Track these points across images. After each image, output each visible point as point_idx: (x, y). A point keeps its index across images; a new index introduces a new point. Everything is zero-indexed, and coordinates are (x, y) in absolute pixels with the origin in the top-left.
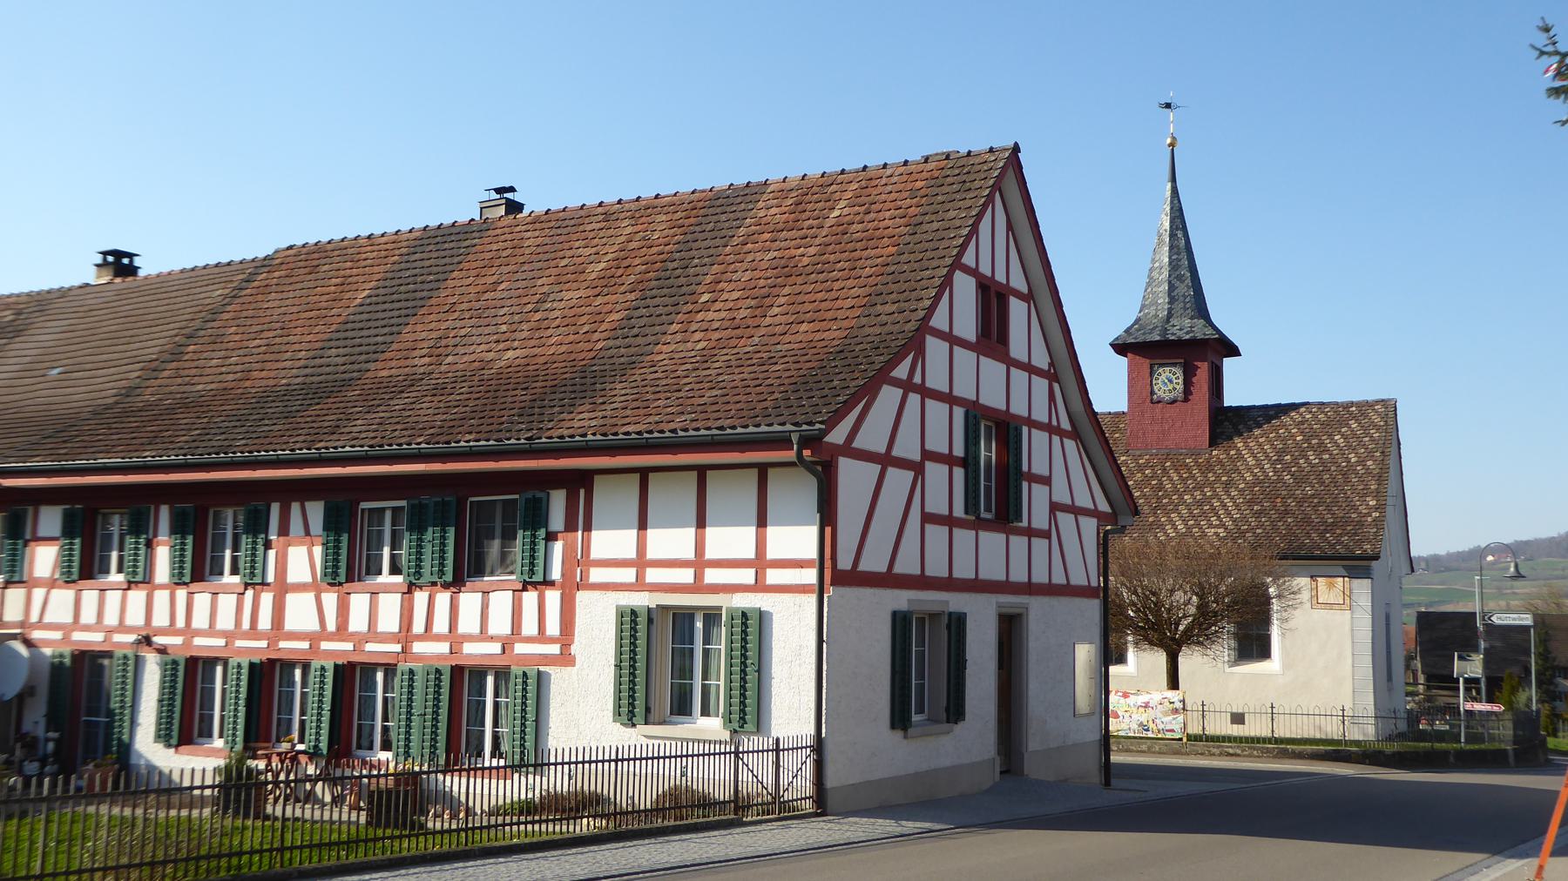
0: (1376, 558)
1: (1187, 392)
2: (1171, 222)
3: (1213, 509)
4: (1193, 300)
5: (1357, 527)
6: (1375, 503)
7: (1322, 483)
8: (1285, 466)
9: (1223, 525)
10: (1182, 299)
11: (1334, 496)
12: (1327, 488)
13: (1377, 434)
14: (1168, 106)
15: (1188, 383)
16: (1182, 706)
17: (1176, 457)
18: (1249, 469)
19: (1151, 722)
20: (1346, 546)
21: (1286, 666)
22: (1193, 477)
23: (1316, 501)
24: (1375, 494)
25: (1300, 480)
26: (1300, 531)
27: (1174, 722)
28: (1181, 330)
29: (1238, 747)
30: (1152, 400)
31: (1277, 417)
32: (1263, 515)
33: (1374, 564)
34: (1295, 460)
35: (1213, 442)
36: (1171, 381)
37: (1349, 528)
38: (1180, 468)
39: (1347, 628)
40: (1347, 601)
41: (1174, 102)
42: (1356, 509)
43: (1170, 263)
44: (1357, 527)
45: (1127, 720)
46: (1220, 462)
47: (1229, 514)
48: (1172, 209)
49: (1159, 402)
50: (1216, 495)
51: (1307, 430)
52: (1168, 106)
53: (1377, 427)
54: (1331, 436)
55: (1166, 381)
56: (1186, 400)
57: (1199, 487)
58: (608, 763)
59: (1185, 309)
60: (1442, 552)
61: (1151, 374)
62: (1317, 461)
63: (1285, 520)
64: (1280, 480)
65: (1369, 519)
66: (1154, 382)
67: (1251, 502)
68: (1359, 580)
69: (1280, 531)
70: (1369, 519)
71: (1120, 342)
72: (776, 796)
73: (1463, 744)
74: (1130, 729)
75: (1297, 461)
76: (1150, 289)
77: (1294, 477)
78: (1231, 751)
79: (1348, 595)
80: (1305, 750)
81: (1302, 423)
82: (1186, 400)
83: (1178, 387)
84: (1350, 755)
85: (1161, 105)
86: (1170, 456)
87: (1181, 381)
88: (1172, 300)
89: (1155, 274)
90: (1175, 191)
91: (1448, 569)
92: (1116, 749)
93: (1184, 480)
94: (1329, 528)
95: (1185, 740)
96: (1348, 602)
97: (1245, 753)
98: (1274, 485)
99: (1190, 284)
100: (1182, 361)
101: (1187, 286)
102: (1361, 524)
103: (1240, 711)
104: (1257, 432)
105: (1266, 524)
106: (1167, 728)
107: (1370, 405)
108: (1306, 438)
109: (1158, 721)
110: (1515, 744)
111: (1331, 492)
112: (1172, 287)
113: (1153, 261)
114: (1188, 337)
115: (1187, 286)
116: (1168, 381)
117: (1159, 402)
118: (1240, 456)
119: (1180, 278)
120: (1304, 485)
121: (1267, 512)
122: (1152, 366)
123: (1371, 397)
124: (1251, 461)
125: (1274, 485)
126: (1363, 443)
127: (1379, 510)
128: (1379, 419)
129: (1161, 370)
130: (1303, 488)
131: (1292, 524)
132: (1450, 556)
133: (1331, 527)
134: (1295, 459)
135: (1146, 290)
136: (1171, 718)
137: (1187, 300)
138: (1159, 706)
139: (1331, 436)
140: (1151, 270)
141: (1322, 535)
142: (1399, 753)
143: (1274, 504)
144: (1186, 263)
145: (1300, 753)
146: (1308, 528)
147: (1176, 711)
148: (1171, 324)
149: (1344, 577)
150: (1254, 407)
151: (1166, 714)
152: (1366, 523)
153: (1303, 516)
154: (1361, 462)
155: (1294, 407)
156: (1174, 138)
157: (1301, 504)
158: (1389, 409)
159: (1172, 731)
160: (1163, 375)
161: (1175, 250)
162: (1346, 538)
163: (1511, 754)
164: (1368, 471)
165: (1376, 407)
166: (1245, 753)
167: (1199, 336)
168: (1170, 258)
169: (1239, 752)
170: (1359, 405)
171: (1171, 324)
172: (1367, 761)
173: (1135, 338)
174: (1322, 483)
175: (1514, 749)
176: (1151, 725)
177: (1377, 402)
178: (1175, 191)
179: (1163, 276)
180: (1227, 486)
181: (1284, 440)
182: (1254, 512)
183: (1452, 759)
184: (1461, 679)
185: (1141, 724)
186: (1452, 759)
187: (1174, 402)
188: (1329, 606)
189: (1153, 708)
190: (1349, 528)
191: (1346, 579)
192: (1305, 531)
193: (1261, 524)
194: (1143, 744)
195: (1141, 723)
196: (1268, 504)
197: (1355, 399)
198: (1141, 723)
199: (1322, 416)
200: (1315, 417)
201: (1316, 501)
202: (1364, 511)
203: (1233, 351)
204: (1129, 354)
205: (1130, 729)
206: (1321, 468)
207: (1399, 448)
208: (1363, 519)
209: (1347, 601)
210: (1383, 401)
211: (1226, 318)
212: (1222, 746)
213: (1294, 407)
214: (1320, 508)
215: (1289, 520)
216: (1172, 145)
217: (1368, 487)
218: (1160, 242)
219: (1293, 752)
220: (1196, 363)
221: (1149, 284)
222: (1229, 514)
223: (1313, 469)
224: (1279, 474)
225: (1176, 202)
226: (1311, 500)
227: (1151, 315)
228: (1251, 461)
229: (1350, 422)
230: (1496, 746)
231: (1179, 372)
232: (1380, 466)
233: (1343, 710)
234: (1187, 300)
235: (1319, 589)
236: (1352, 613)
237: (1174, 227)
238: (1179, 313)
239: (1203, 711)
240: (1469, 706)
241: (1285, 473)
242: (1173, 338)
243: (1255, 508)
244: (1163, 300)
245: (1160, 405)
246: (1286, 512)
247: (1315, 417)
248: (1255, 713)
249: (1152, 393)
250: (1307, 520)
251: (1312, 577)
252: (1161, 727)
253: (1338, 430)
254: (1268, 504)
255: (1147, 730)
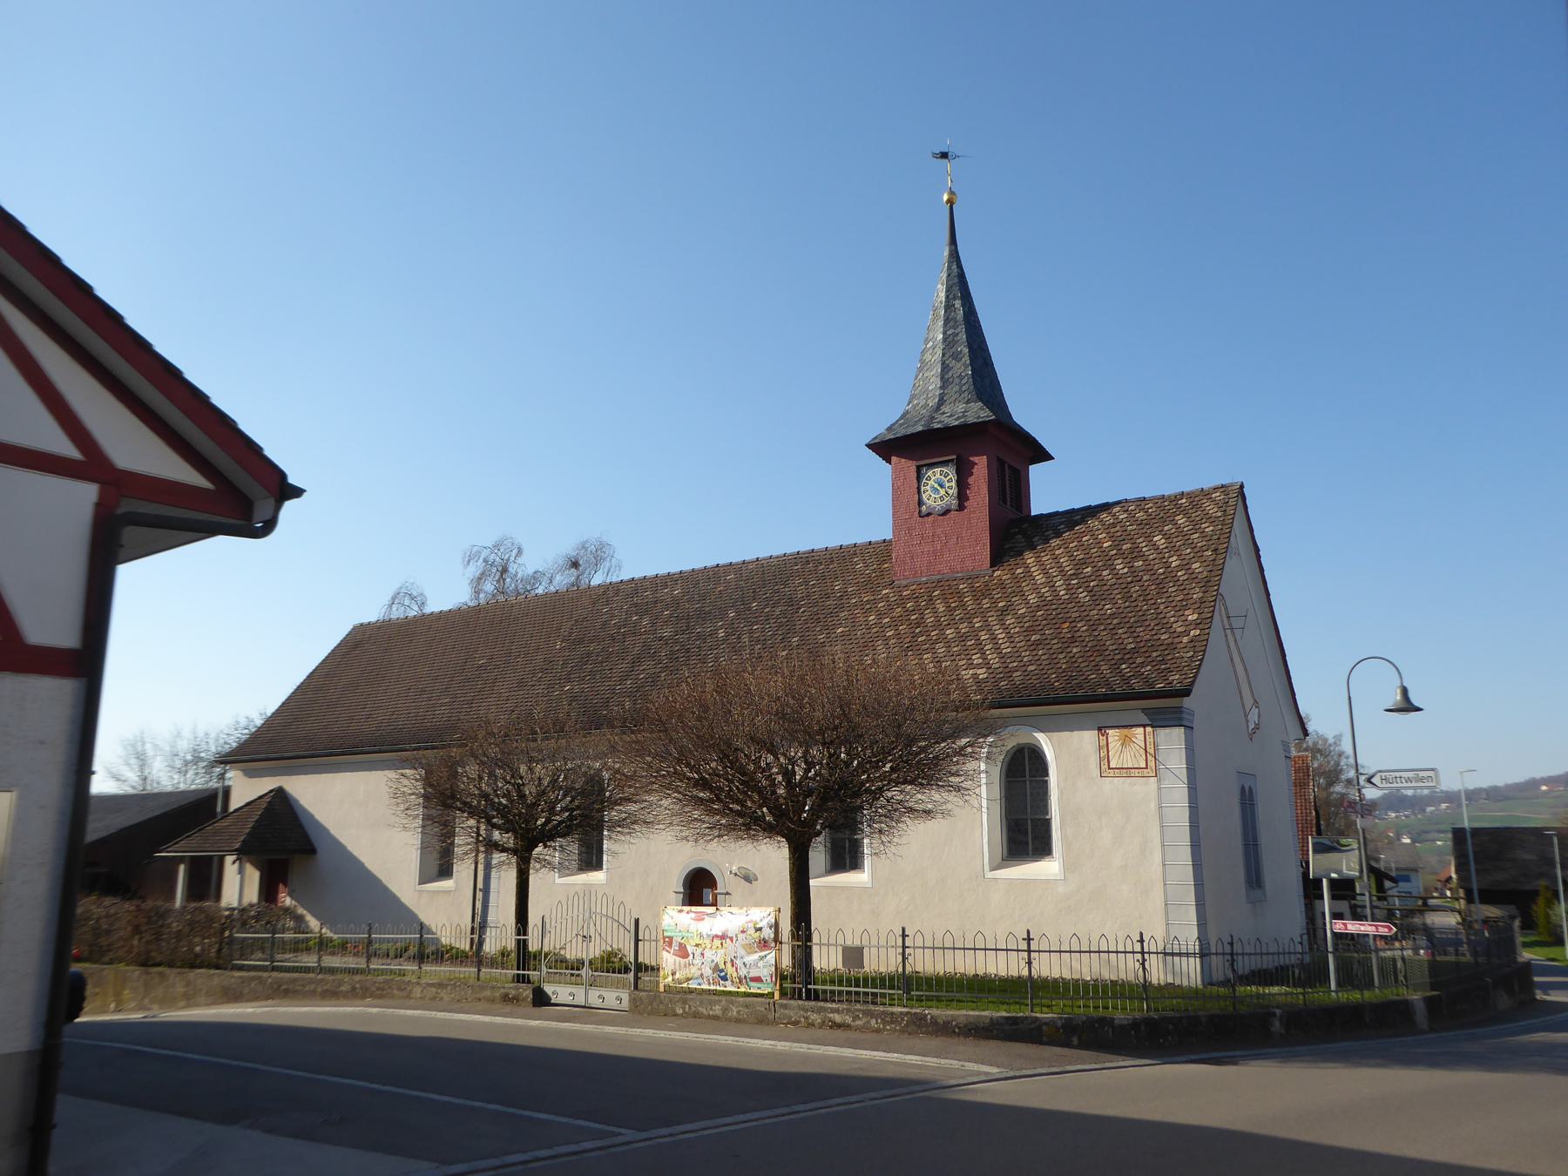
0: (1186, 692)
1: (962, 497)
2: (947, 291)
3: (979, 644)
4: (971, 380)
5: (1166, 652)
6: (1195, 616)
7: (1127, 597)
8: (1082, 580)
9: (987, 665)
10: (957, 380)
11: (1141, 613)
12: (1134, 604)
13: (1211, 528)
14: (944, 155)
15: (962, 485)
16: (772, 936)
17: (947, 583)
18: (1036, 589)
19: (729, 965)
20: (1146, 680)
21: (1068, 867)
22: (963, 606)
23: (1115, 621)
24: (1196, 606)
25: (1097, 598)
26: (1086, 664)
27: (761, 964)
28: (951, 416)
29: (848, 1010)
30: (920, 512)
31: (1083, 521)
32: (1041, 647)
33: (1187, 702)
34: (1097, 573)
35: (997, 559)
36: (942, 486)
37: (1155, 654)
38: (949, 596)
39: (1153, 805)
40: (1152, 764)
41: (952, 151)
42: (1168, 627)
43: (945, 340)
44: (1166, 652)
45: (698, 961)
46: (1002, 585)
47: (997, 648)
48: (949, 275)
49: (929, 514)
50: (987, 627)
51: (1119, 534)
52: (944, 155)
53: (1213, 519)
54: (1149, 538)
55: (936, 485)
56: (961, 507)
57: (969, 618)
58: (1222, 957)
59: (961, 392)
60: (1500, 783)
61: (919, 479)
62: (1126, 570)
63: (1069, 650)
64: (1073, 598)
65: (1185, 640)
66: (922, 489)
67: (1030, 630)
68: (1167, 730)
69: (1059, 665)
70: (1185, 640)
71: (877, 441)
72: (1144, 986)
73: (1377, 990)
74: (702, 975)
75: (1099, 573)
76: (921, 374)
77: (1092, 593)
78: (838, 1018)
79: (1151, 753)
80: (954, 1018)
81: (1114, 525)
82: (961, 507)
83: (950, 492)
84: (1040, 1027)
85: (935, 156)
86: (941, 584)
87: (953, 484)
88: (945, 382)
89: (928, 357)
90: (955, 256)
91: (1507, 798)
92: (681, 1011)
93: (950, 610)
94: (1128, 656)
95: (777, 996)
96: (1153, 764)
97: (859, 1023)
98: (1063, 606)
99: (968, 362)
100: (955, 457)
101: (964, 364)
102: (1172, 647)
103: (857, 943)
104: (1055, 542)
105: (1043, 657)
106: (752, 975)
107: (1205, 493)
108: (1116, 543)
109: (738, 962)
110: (1433, 987)
111: (1138, 609)
112: (945, 368)
113: (927, 341)
114: (957, 423)
115: (964, 364)
116: (939, 485)
117: (929, 514)
118: (1028, 573)
119: (956, 357)
120: (1103, 603)
121: (1047, 642)
122: (919, 469)
123: (1207, 484)
124: (1040, 579)
125: (1063, 606)
126: (1190, 541)
127: (1201, 626)
128: (1216, 510)
129: (930, 473)
130: (1101, 607)
131: (1077, 655)
132: (1509, 787)
133: (1128, 656)
134: (1097, 570)
135: (917, 377)
136: (756, 956)
137: (964, 382)
138: (741, 936)
139: (1149, 538)
140: (923, 353)
141: (1115, 667)
142: (1148, 1022)
143: (1059, 631)
144: (964, 336)
145: (946, 1023)
146: (1098, 659)
147: (763, 944)
148: (942, 411)
149: (1144, 726)
150: (1056, 514)
151: (750, 949)
152: (1182, 645)
153: (1095, 643)
154: (1185, 566)
155: (1106, 508)
156: (952, 193)
157: (1094, 627)
158: (1238, 495)
159: (758, 979)
160: (933, 478)
161: (952, 323)
162: (1148, 668)
163: (1420, 1008)
164: (1192, 576)
165: (1213, 496)
166: (859, 1023)
167: (971, 419)
168: (944, 333)
169: (848, 1019)
170: (1190, 496)
171: (942, 411)
172: (1075, 1040)
173: (895, 434)
174: (1127, 597)
175: (1428, 1000)
176: (730, 970)
177: (1216, 489)
178: (955, 256)
179: (936, 357)
180: (1003, 612)
181: (1086, 549)
182: (1030, 643)
183: (1277, 1026)
184: (1324, 881)
185: (716, 969)
186: (1277, 1026)
187: (947, 512)
188: (1125, 772)
189: (731, 939)
190: (1155, 654)
191: (1149, 729)
192: (1093, 664)
193: (1037, 658)
194: (716, 1002)
195: (717, 965)
196: (1051, 631)
197: (1186, 489)
198: (717, 965)
199: (1142, 514)
200: (1131, 515)
201: (1115, 621)
202: (1179, 630)
203: (1042, 455)
204: (894, 459)
205: (702, 975)
206: (1129, 579)
207: (1259, 557)
208: (1177, 640)
209: (1152, 764)
210: (1223, 486)
211: (1025, 413)
212: (825, 1010)
213: (1106, 507)
214: (1120, 631)
215: (1075, 650)
216: (950, 202)
217: (1190, 596)
218: (935, 318)
219: (934, 1021)
220: (972, 459)
221: (920, 370)
222: (997, 648)
223: (1120, 581)
224: (1073, 591)
225: (955, 267)
226: (1109, 621)
227: (920, 405)
228: (1040, 579)
229: (1177, 518)
230: (1391, 994)
231: (952, 475)
232: (1209, 568)
233: (1142, 941)
234: (964, 382)
235: (1111, 746)
236: (1159, 781)
237: (951, 296)
238: (953, 398)
239: (904, 947)
240: (1339, 926)
241: (1081, 590)
242: (939, 426)
243: (1033, 638)
244: (934, 384)
245: (930, 519)
246: (1073, 640)
247: (1131, 515)
248: (924, 948)
249: (920, 503)
250: (1099, 649)
251: (1099, 729)
252: (743, 972)
253: (1160, 529)
254: (1051, 631)
255: (725, 978)
